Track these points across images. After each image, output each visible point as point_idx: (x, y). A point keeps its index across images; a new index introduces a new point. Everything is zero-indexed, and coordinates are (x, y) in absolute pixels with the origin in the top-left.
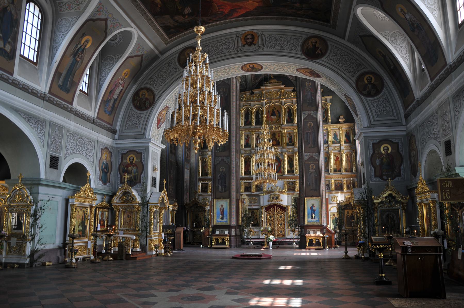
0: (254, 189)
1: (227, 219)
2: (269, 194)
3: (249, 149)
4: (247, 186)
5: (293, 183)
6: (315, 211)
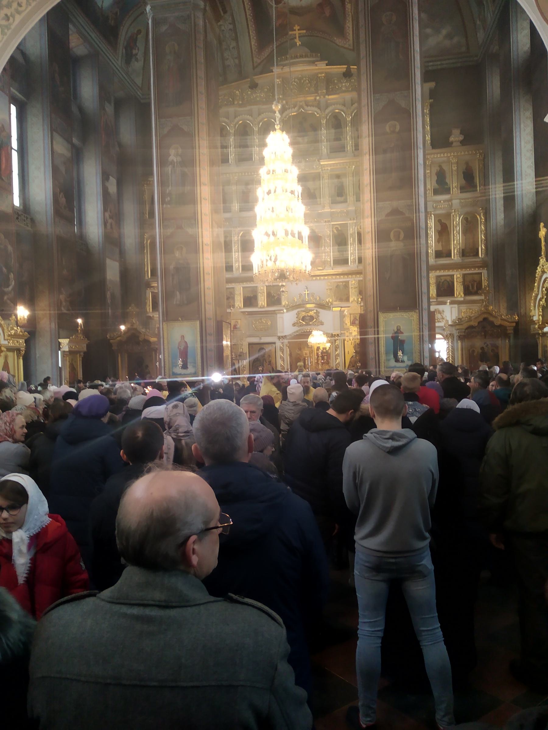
0: (262, 300)
1: (194, 367)
2: (295, 311)
3: (446, 197)
4: (249, 295)
5: (346, 285)
6: (402, 342)
